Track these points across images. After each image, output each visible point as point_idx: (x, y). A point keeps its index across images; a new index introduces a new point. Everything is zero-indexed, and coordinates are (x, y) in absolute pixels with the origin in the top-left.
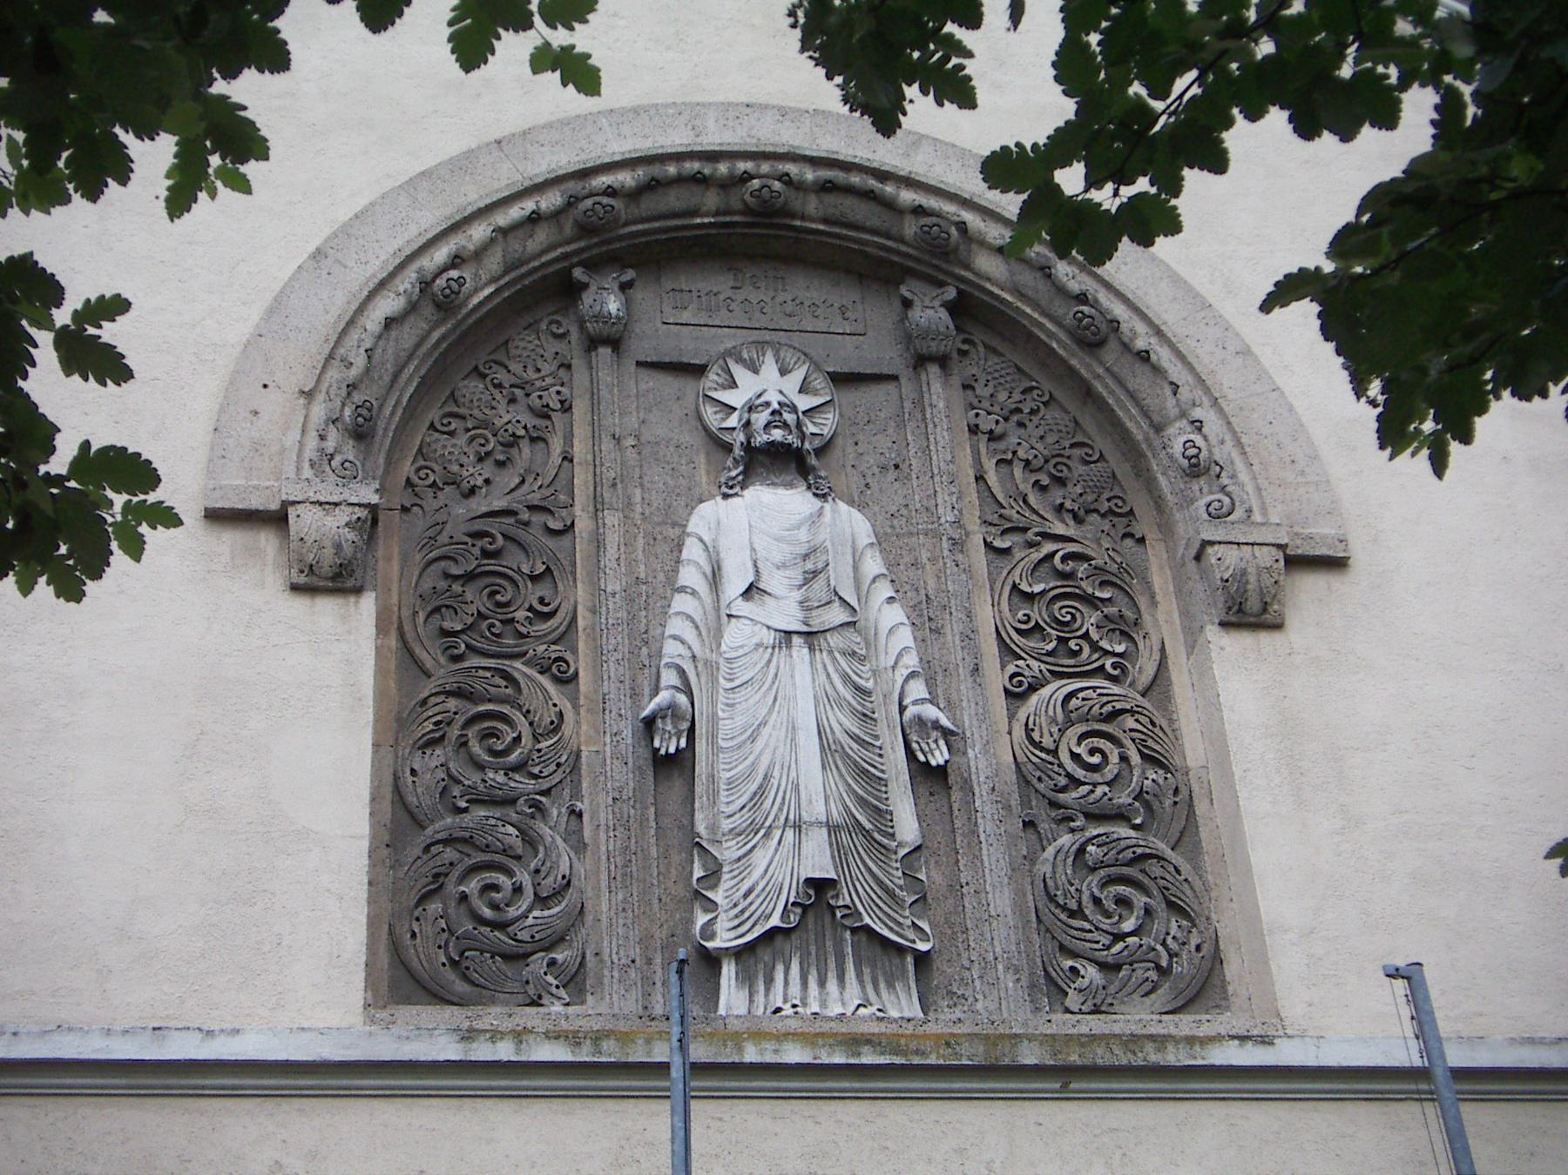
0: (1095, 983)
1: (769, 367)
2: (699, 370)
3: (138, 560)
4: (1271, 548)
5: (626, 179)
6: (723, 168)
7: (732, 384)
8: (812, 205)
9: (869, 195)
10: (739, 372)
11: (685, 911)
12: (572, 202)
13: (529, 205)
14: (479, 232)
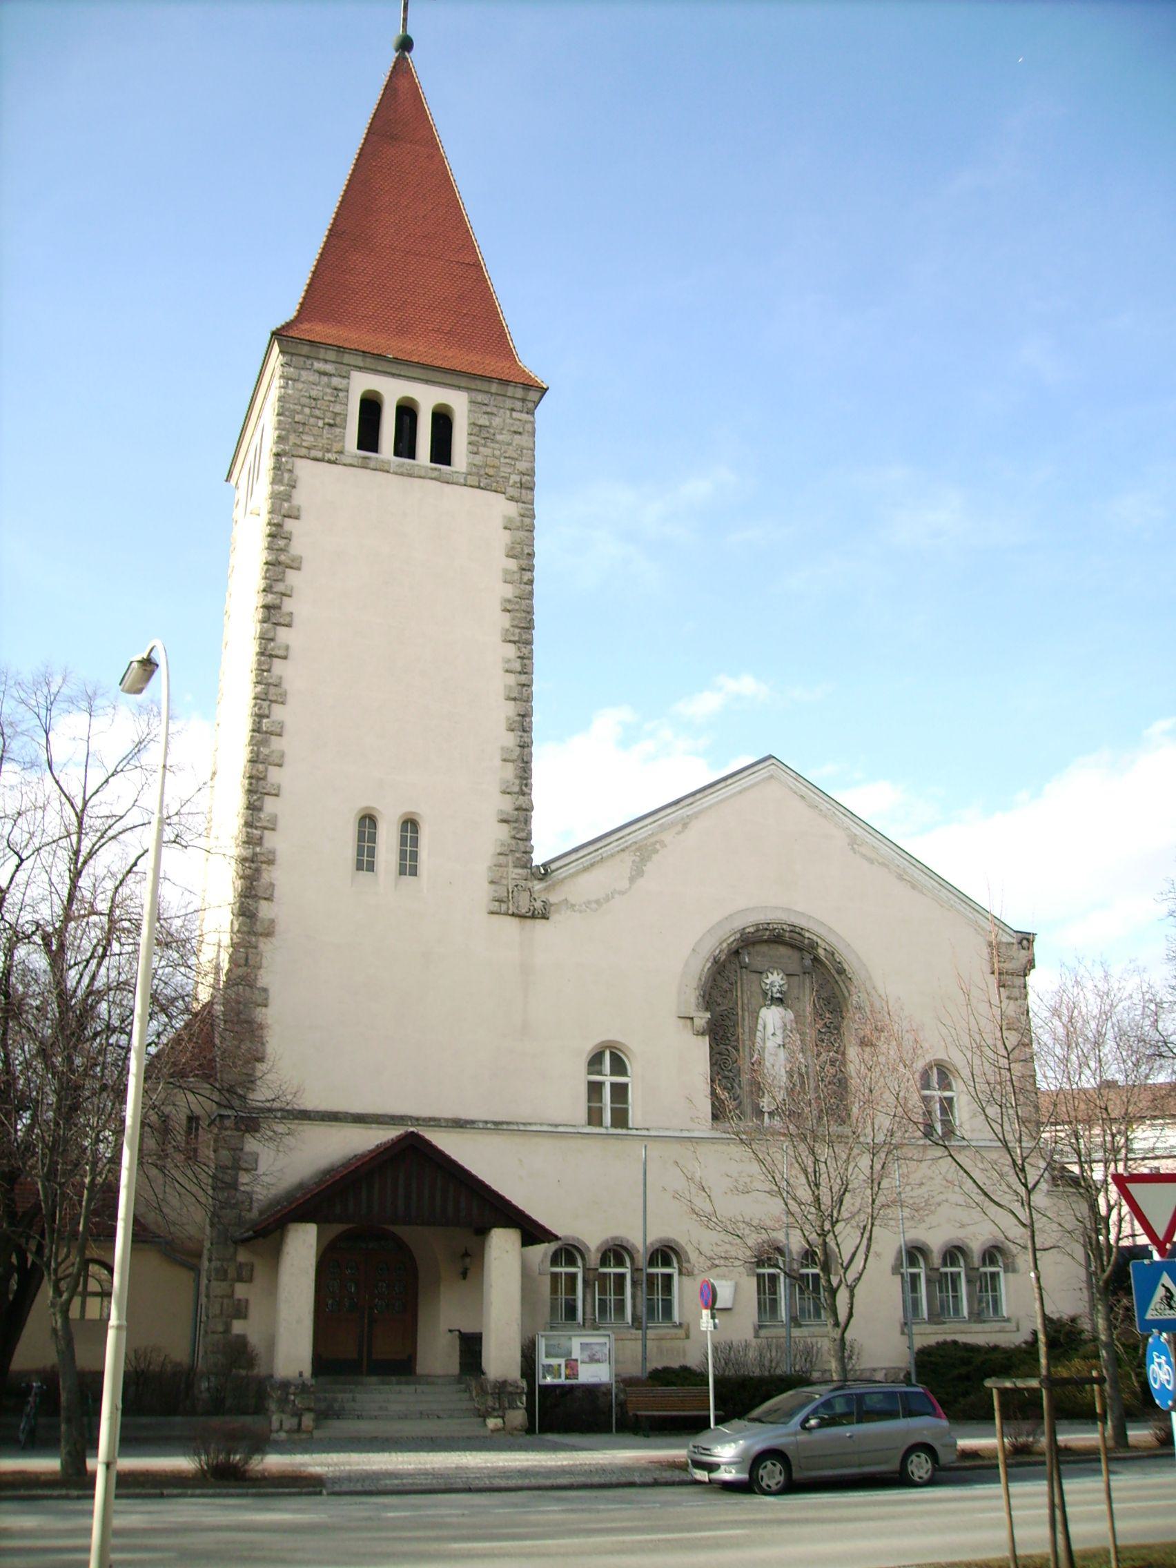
0: (787, 1021)
1: (775, 973)
2: (761, 973)
4: (283, 622)
7: (767, 978)
8: (787, 934)
9: (799, 934)
10: (769, 975)
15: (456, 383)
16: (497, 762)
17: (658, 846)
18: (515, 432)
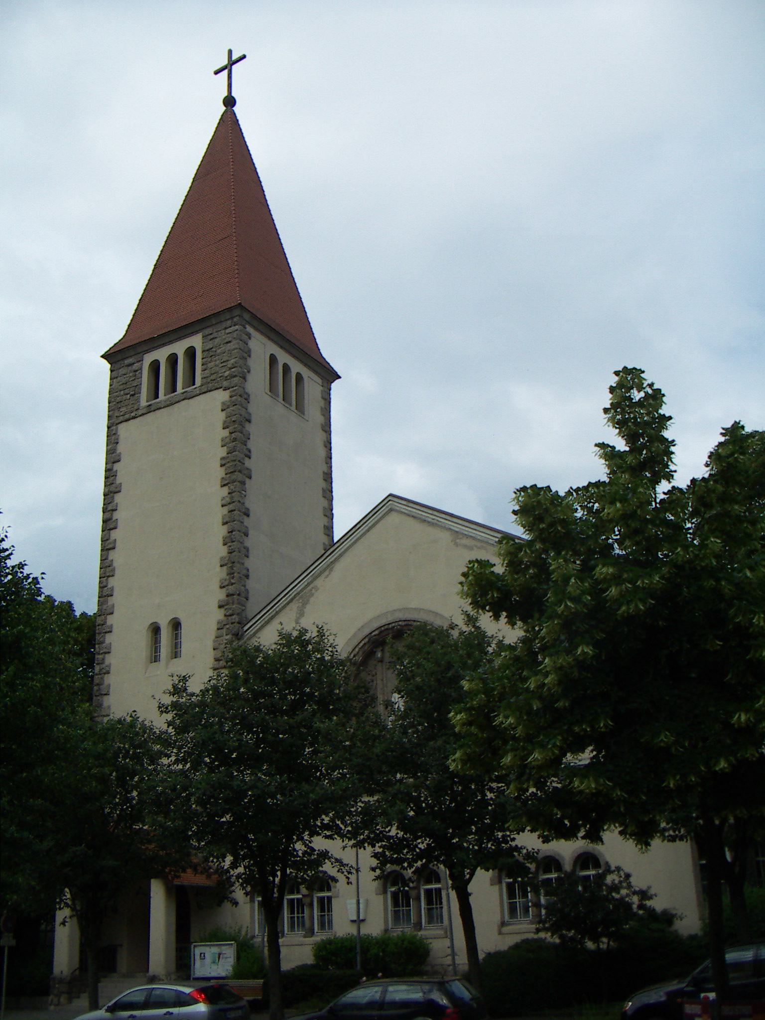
3: (102, 357)
5: (377, 632)
6: (390, 626)
11: (225, 696)
12: (369, 639)
13: (363, 642)
14: (357, 650)
15: (160, 343)
16: (218, 569)
17: (313, 591)
18: (227, 343)
